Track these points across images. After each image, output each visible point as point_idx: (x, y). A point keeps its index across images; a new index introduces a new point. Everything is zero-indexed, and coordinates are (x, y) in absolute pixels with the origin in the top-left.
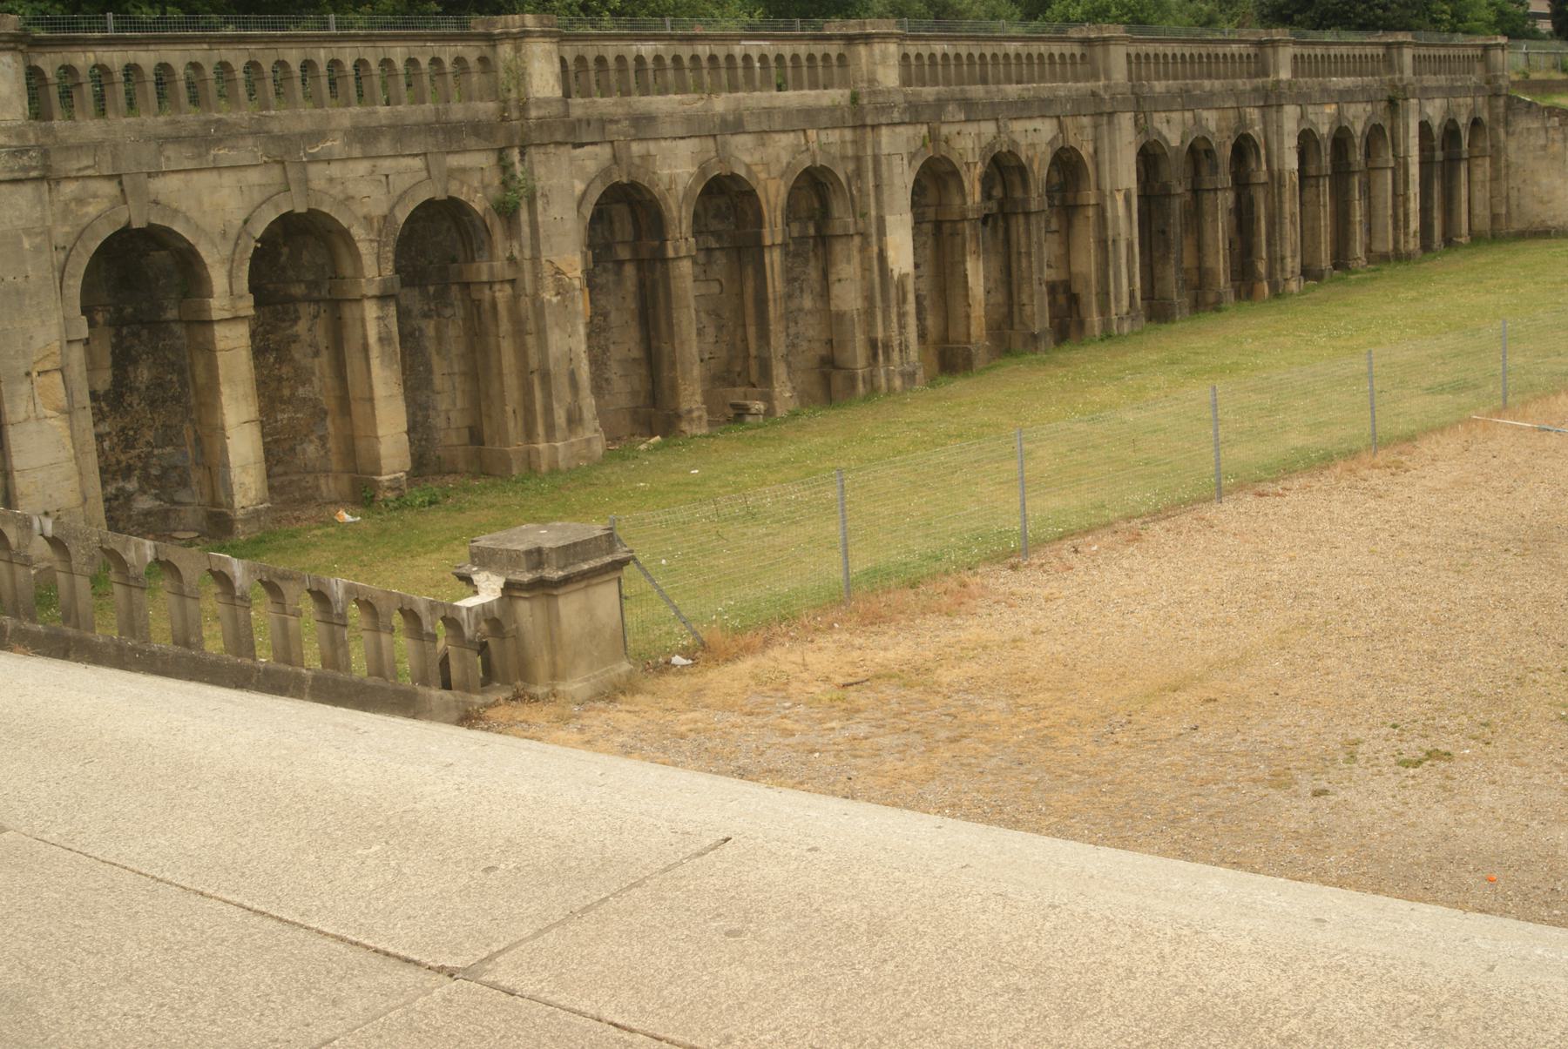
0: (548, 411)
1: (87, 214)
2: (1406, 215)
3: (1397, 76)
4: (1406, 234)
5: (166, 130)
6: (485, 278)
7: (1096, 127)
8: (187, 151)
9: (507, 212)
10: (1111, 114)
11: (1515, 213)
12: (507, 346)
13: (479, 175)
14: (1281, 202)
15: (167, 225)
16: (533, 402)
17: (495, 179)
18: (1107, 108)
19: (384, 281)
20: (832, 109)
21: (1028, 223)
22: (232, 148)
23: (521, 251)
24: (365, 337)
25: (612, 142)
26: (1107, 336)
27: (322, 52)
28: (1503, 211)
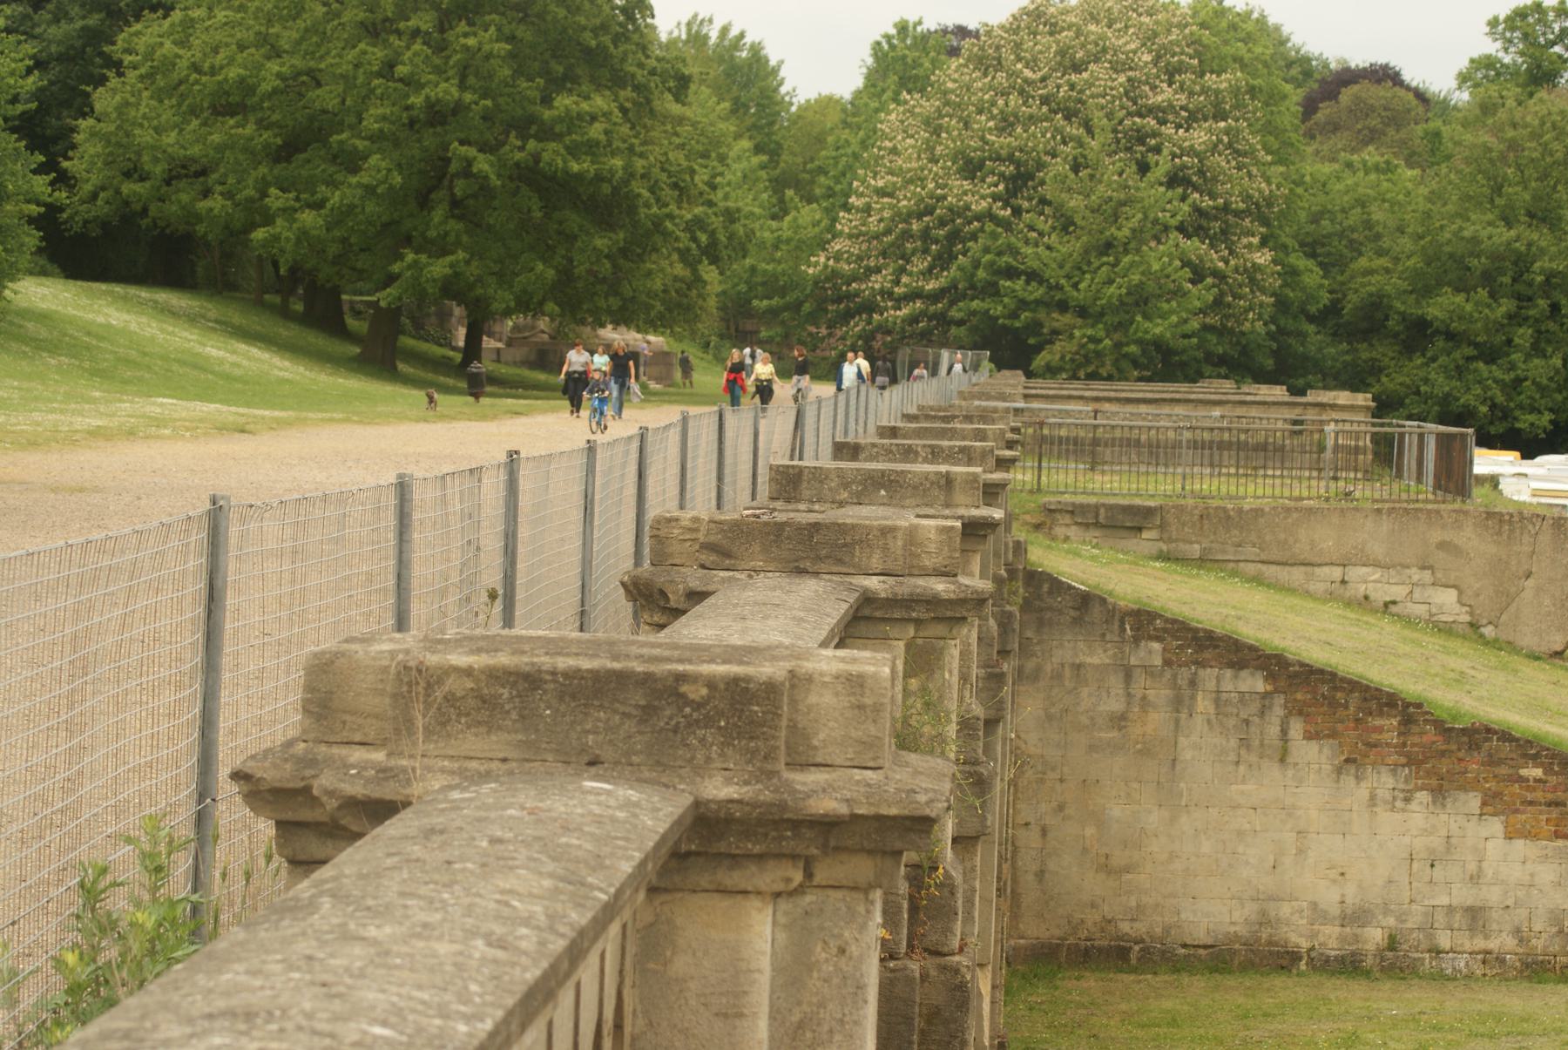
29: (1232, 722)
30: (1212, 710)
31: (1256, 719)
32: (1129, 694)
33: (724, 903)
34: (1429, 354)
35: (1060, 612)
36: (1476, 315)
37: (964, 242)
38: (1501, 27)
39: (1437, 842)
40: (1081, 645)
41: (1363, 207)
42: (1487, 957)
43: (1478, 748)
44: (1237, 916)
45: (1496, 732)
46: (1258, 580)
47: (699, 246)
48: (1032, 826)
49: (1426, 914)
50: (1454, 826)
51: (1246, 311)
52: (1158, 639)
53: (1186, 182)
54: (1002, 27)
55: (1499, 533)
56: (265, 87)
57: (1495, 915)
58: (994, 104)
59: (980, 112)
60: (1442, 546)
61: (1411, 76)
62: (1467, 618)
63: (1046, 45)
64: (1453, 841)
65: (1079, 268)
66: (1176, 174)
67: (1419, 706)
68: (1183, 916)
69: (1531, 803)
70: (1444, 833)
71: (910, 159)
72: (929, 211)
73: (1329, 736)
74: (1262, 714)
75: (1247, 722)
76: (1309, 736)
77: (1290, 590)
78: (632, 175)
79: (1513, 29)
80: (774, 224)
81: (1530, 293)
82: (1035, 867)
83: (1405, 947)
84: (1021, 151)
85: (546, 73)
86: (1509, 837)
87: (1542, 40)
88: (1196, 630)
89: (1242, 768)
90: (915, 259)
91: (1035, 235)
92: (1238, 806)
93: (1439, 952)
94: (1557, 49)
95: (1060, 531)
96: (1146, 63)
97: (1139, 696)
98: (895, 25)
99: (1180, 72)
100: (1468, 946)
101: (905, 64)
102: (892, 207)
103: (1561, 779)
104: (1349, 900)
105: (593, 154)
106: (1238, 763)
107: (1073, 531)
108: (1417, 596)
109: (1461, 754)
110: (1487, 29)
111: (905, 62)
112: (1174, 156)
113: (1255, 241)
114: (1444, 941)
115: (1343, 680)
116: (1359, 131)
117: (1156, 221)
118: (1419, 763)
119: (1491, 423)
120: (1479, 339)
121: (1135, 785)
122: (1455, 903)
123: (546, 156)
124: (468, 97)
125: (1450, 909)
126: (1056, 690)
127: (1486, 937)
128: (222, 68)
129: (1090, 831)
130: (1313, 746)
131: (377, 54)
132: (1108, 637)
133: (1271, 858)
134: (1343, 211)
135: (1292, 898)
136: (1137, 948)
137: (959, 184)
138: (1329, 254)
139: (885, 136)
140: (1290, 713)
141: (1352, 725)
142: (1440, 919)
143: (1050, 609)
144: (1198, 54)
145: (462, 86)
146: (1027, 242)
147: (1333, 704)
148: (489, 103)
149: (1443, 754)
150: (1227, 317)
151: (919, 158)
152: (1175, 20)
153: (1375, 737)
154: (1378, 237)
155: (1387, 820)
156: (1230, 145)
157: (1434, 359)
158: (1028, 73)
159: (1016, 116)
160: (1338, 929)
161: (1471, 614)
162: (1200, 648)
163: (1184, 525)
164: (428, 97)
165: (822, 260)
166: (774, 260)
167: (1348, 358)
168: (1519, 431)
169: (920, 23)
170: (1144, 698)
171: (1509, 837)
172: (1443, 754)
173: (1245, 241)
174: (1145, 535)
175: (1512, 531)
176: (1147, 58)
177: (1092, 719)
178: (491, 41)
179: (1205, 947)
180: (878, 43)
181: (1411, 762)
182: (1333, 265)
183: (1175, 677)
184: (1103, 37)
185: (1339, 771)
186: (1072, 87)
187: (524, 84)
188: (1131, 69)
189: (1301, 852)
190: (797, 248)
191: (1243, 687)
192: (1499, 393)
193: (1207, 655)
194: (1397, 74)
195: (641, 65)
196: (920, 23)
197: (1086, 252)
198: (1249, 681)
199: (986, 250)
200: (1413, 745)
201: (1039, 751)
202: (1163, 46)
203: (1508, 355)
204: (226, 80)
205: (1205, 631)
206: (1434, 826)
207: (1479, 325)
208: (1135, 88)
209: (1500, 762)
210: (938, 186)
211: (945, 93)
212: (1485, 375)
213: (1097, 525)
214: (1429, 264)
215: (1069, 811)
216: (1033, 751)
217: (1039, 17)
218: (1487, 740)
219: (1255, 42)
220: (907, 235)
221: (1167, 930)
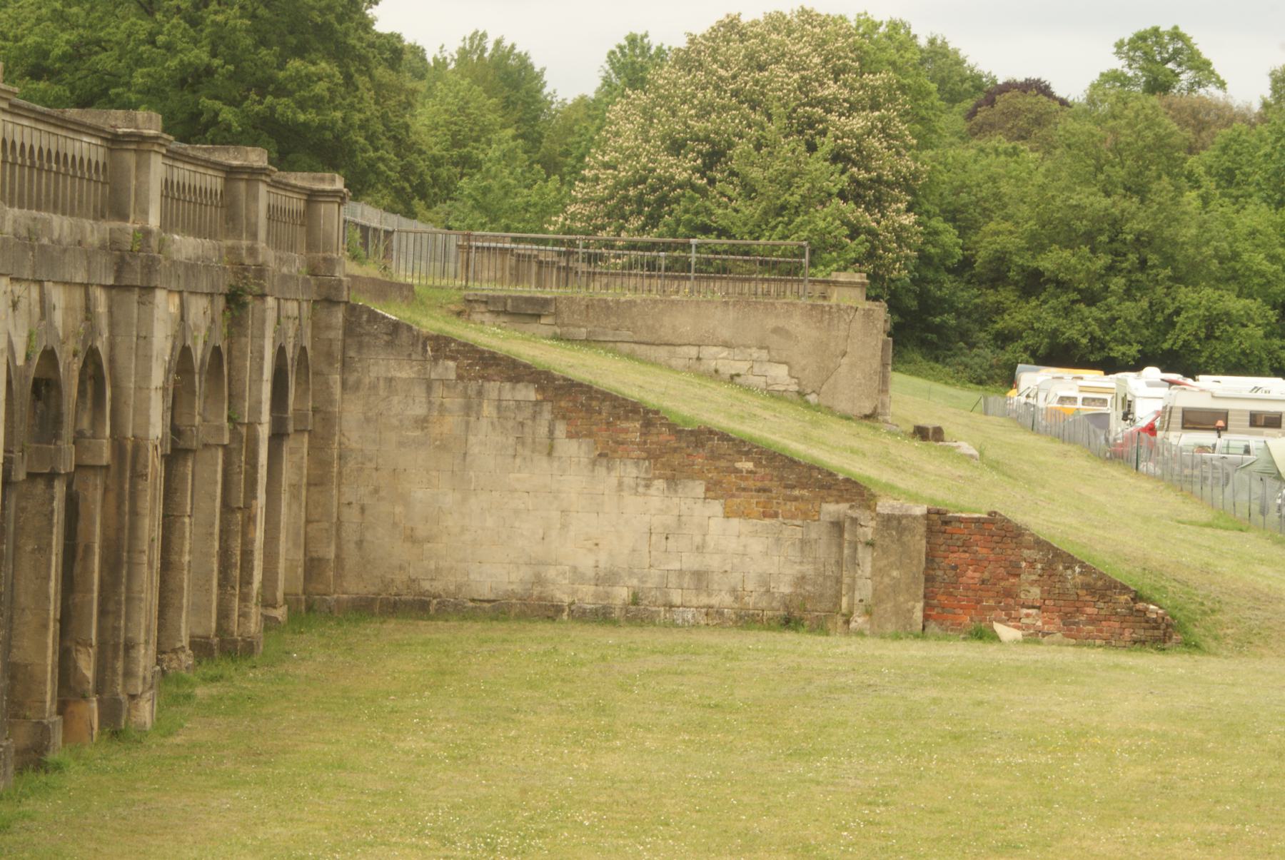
2: (247, 554)
3: (245, 243)
4: (245, 598)
11: (351, 560)
14: (135, 513)
29: (510, 424)
30: (495, 414)
31: (529, 422)
32: (430, 402)
34: (1042, 298)
35: (376, 337)
36: (1079, 267)
37: (669, 205)
38: (1125, 48)
39: (670, 520)
40: (392, 362)
41: (994, 182)
42: (709, 611)
43: (703, 446)
44: (514, 577)
45: (717, 434)
46: (631, 356)
47: (411, 186)
48: (354, 505)
49: (662, 576)
50: (683, 507)
51: (894, 262)
52: (453, 359)
53: (847, 159)
54: (703, 36)
55: (821, 321)
56: (57, 52)
57: (716, 578)
58: (694, 96)
59: (684, 103)
60: (776, 330)
61: (1059, 91)
62: (796, 388)
63: (737, 49)
64: (683, 519)
65: (759, 226)
66: (838, 154)
67: (657, 412)
68: (472, 577)
69: (744, 489)
70: (676, 512)
71: (628, 139)
72: (643, 180)
73: (586, 436)
74: (534, 418)
75: (522, 424)
76: (570, 436)
77: (654, 363)
78: (351, 126)
79: (1135, 49)
80: (526, 191)
81: (1125, 250)
82: (355, 538)
83: (646, 602)
84: (716, 133)
85: (283, 44)
86: (727, 516)
87: (1158, 58)
88: (483, 352)
89: (518, 461)
90: (631, 219)
91: (725, 199)
92: (516, 490)
93: (671, 606)
94: (1170, 66)
95: (476, 317)
96: (816, 65)
97: (438, 403)
98: (627, 38)
99: (844, 72)
100: (694, 602)
101: (634, 69)
102: (615, 177)
103: (768, 470)
104: (602, 565)
105: (319, 108)
106: (515, 456)
107: (487, 317)
108: (756, 370)
109: (689, 451)
110: (1115, 50)
111: (632, 65)
112: (837, 138)
113: (902, 206)
114: (676, 598)
115: (597, 391)
116: (1010, 129)
117: (821, 190)
118: (657, 458)
119: (1092, 352)
120: (1081, 286)
121: (434, 473)
122: (684, 567)
123: (279, 109)
124: (217, 62)
125: (681, 573)
126: (372, 399)
127: (709, 595)
128: (23, 36)
129: (398, 509)
130: (574, 443)
131: (145, 26)
132: (414, 357)
133: (541, 532)
134: (978, 185)
135: (557, 563)
136: (435, 602)
137: (665, 159)
138: (966, 219)
139: (611, 123)
140: (556, 417)
141: (604, 427)
142: (673, 580)
143: (368, 334)
144: (859, 59)
145: (214, 55)
146: (719, 205)
147: (589, 410)
148: (231, 67)
149: (675, 450)
150: (879, 267)
151: (636, 139)
152: (842, 32)
153: (622, 436)
154: (1005, 206)
155: (632, 502)
156: (883, 130)
157: (1045, 302)
158: (722, 72)
159: (712, 106)
160: (593, 588)
161: (799, 384)
162: (486, 365)
163: (573, 313)
164: (182, 61)
165: (561, 219)
166: (524, 220)
167: (978, 301)
168: (1114, 358)
169: (646, 36)
170: (442, 404)
171: (727, 516)
172: (675, 450)
173: (894, 206)
174: (543, 321)
175: (831, 319)
176: (816, 60)
177: (401, 421)
178: (235, 18)
179: (489, 601)
180: (613, 53)
181: (652, 456)
182: (970, 229)
183: (466, 388)
184: (782, 44)
185: (594, 463)
186: (756, 82)
187: (263, 52)
188: (804, 69)
189: (564, 526)
190: (542, 210)
191: (519, 396)
192: (1097, 329)
193: (491, 371)
194: (1047, 87)
195: (361, 39)
196: (646, 36)
197: (765, 213)
198: (524, 392)
199: (686, 211)
200: (652, 443)
201: (359, 446)
202: (830, 52)
203: (1105, 299)
204: (25, 45)
205: (490, 352)
206: (668, 507)
207: (1082, 275)
208: (807, 84)
209: (720, 457)
210: (650, 161)
211: (657, 88)
212: (1087, 314)
213: (505, 313)
214: (1043, 227)
215: (383, 493)
216: (354, 445)
217: (733, 28)
218: (709, 439)
219: (906, 50)
220: (626, 199)
221: (459, 587)
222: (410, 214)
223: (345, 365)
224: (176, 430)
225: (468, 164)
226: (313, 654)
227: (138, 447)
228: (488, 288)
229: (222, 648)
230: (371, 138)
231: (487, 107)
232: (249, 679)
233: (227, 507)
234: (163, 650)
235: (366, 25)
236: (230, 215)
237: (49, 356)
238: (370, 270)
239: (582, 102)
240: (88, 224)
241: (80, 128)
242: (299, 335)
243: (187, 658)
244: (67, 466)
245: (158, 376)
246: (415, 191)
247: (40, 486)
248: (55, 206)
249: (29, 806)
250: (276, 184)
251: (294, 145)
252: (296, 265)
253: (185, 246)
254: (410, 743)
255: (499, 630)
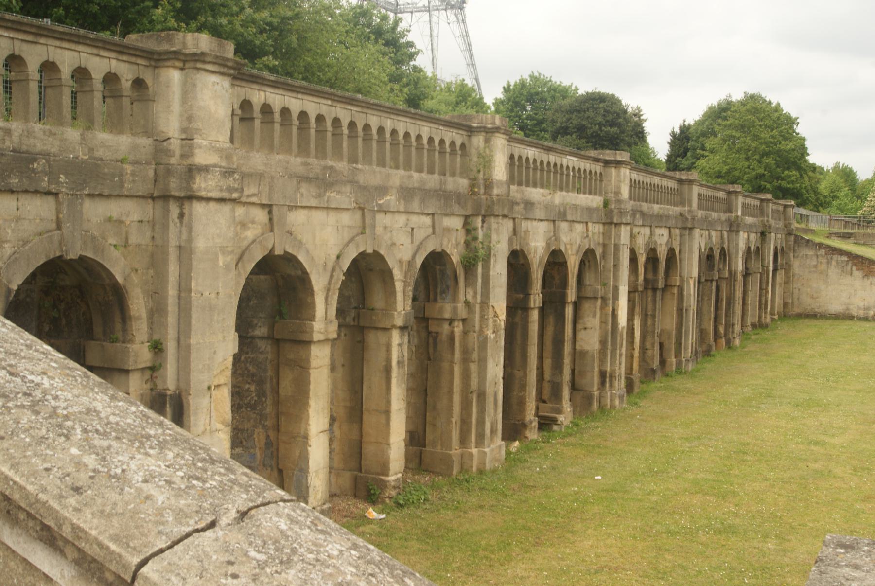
0: (481, 422)
1: (246, 238)
2: (766, 301)
4: (766, 313)
5: (301, 170)
6: (447, 315)
7: (681, 236)
8: (314, 191)
9: (469, 266)
10: (691, 229)
11: (796, 303)
12: (457, 370)
13: (455, 234)
14: (734, 290)
15: (294, 253)
16: (470, 415)
17: (461, 237)
18: (689, 225)
19: (406, 314)
20: (590, 210)
21: (654, 296)
22: (339, 192)
23: (475, 296)
24: (389, 360)
25: (514, 219)
26: (679, 371)
27: (389, 121)
28: (790, 301)
33: (195, 71)
131: (747, 164)
222: (818, 211)
223: (794, 251)
224: (747, 269)
225: (835, 197)
226: (784, 328)
227: (735, 273)
228: (836, 230)
229: (759, 326)
230: (807, 191)
231: (840, 182)
232: (766, 334)
233: (761, 288)
234: (743, 326)
235: (806, 161)
236: (762, 211)
237: (711, 249)
238: (803, 226)
239: (867, 180)
240: (722, 214)
241: (720, 190)
242: (781, 243)
243: (750, 328)
244: (716, 277)
245: (740, 254)
246: (820, 205)
247: (709, 283)
248: (713, 210)
249: (705, 365)
250: (775, 203)
251: (783, 193)
252: (781, 224)
253: (749, 220)
254: (809, 352)
255: (837, 322)
